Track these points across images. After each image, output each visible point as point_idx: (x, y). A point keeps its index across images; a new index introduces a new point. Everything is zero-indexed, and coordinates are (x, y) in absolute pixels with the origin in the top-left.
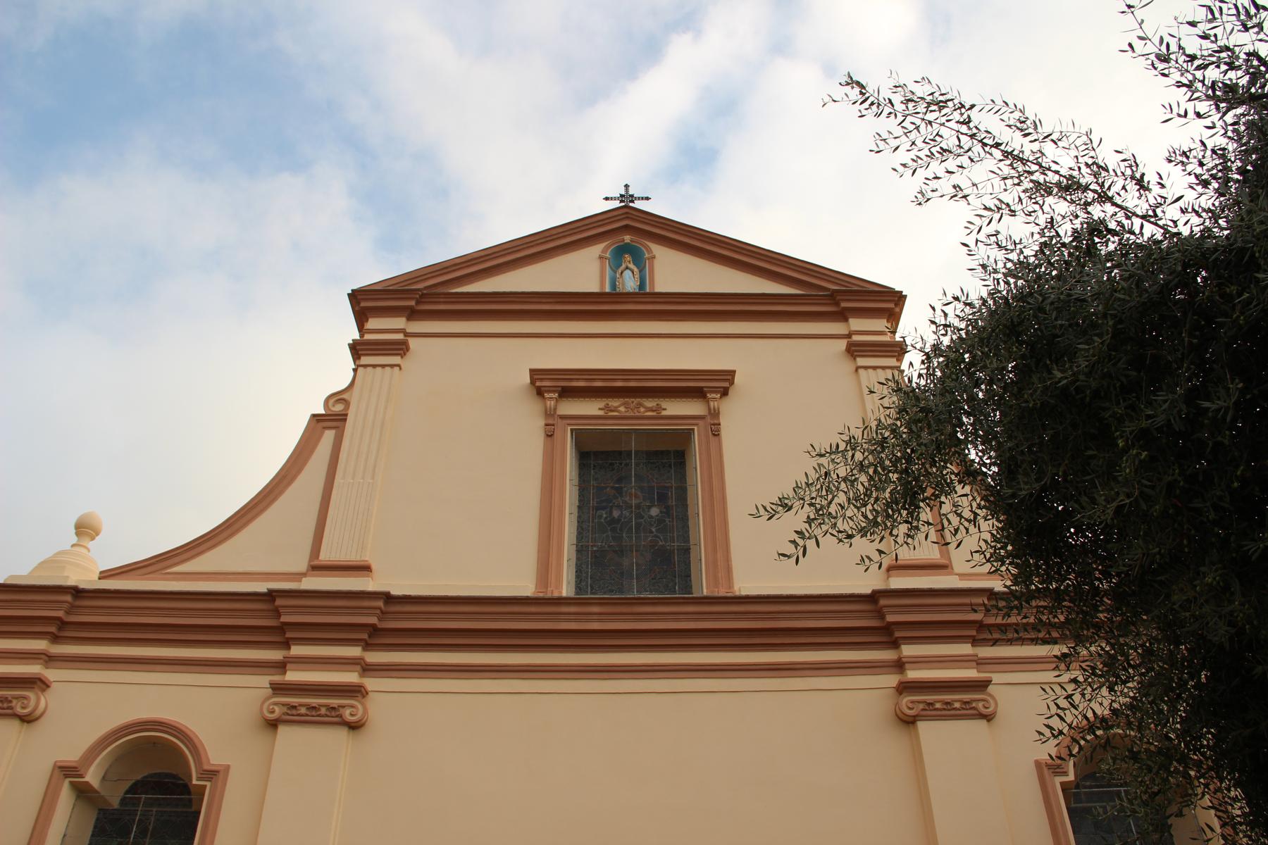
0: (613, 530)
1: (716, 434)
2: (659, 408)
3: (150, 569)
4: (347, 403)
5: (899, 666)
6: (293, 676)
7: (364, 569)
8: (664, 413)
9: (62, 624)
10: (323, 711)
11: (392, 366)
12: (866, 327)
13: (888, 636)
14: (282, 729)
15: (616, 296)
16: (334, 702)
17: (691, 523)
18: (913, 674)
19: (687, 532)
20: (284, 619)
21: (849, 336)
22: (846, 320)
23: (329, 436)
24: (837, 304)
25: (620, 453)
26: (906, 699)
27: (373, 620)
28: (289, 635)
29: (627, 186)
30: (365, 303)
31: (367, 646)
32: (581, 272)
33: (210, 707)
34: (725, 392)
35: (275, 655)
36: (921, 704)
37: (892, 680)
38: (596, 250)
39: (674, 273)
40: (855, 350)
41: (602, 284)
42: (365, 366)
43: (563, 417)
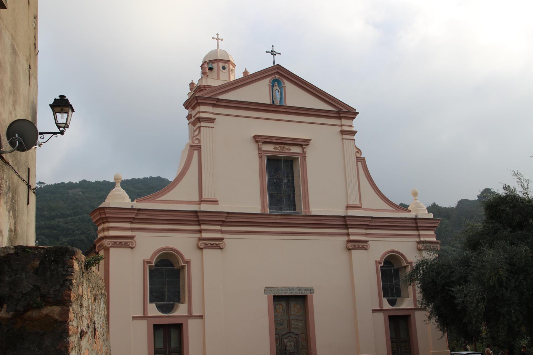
1: (305, 160)
2: (289, 149)
3: (151, 199)
5: (419, 236)
6: (204, 235)
7: (215, 202)
8: (291, 151)
10: (209, 245)
11: (212, 127)
13: (346, 226)
18: (352, 238)
21: (341, 126)
23: (196, 153)
24: (339, 114)
26: (350, 244)
27: (134, 216)
29: (273, 46)
32: (260, 93)
35: (197, 228)
36: (354, 246)
37: (346, 238)
39: (295, 97)
40: (343, 132)
43: (264, 151)
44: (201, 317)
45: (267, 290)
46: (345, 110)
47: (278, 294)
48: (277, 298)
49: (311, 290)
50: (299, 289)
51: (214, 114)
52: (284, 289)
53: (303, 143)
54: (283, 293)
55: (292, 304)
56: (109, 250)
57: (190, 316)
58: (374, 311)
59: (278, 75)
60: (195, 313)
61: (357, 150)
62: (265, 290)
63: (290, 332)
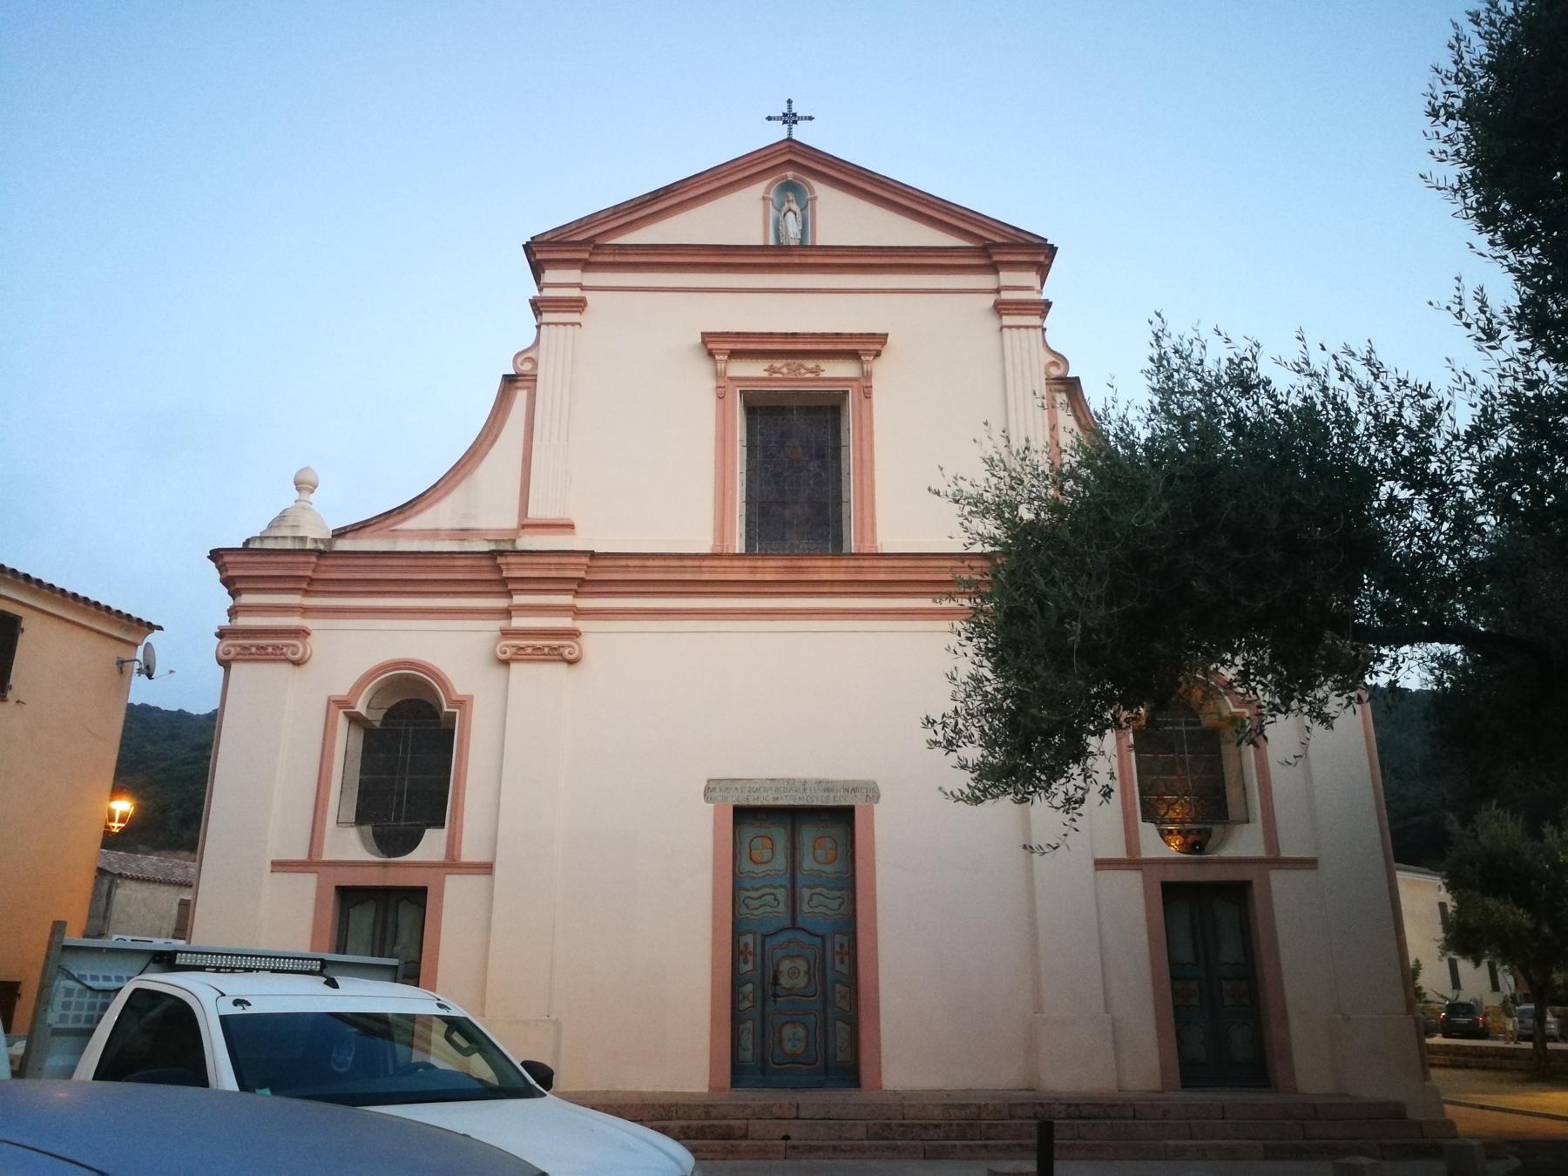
0: (777, 483)
1: (868, 396)
2: (817, 370)
4: (534, 362)
6: (518, 622)
8: (823, 375)
9: (311, 580)
10: (529, 650)
11: (573, 324)
12: (1017, 280)
14: (513, 666)
15: (780, 249)
16: (555, 643)
17: (844, 478)
19: (1179, 1048)
20: (505, 574)
21: (998, 291)
22: (997, 272)
24: (989, 256)
25: (783, 408)
27: (582, 574)
28: (510, 587)
29: (790, 102)
30: (543, 253)
31: (577, 594)
33: (450, 646)
34: (878, 354)
35: (501, 603)
38: (758, 189)
39: (841, 220)
40: (1001, 308)
41: (766, 236)
42: (548, 324)
43: (732, 379)
44: (487, 868)
45: (712, 789)
46: (998, 240)
47: (752, 803)
48: (744, 815)
49: (871, 792)
50: (827, 786)
51: (583, 288)
52: (774, 785)
53: (862, 347)
54: (767, 799)
55: (808, 834)
56: (739, 1073)
57: (452, 864)
58: (1101, 864)
59: (794, 166)
60: (468, 854)
61: (1052, 358)
62: (707, 789)
63: (794, 927)
